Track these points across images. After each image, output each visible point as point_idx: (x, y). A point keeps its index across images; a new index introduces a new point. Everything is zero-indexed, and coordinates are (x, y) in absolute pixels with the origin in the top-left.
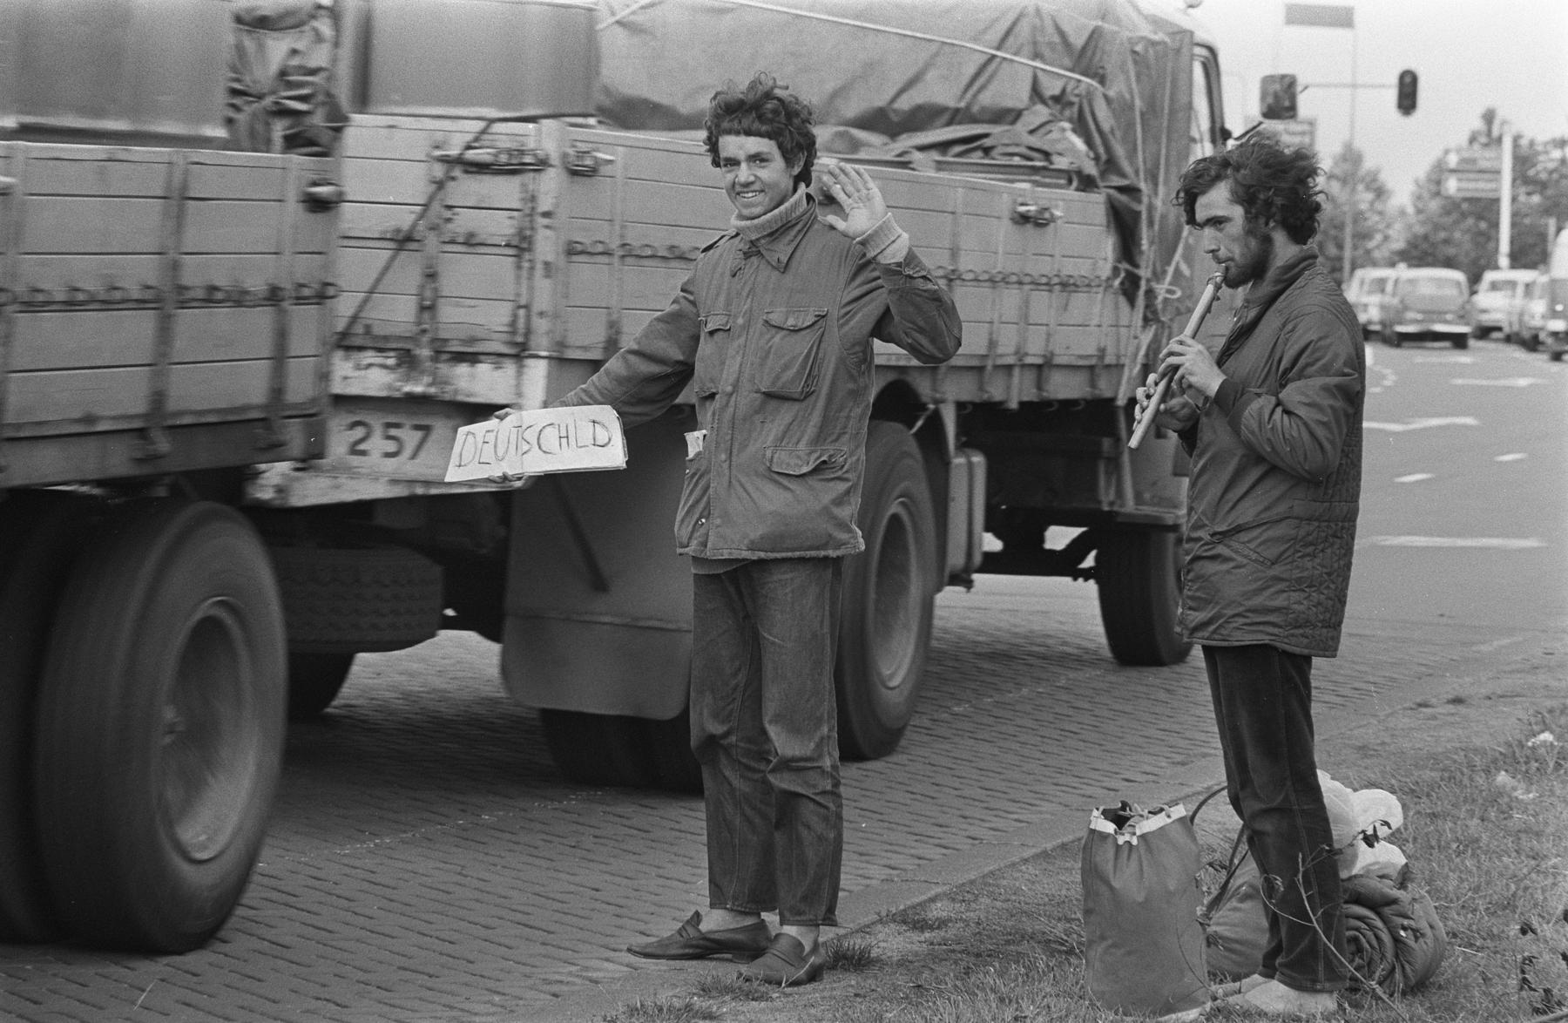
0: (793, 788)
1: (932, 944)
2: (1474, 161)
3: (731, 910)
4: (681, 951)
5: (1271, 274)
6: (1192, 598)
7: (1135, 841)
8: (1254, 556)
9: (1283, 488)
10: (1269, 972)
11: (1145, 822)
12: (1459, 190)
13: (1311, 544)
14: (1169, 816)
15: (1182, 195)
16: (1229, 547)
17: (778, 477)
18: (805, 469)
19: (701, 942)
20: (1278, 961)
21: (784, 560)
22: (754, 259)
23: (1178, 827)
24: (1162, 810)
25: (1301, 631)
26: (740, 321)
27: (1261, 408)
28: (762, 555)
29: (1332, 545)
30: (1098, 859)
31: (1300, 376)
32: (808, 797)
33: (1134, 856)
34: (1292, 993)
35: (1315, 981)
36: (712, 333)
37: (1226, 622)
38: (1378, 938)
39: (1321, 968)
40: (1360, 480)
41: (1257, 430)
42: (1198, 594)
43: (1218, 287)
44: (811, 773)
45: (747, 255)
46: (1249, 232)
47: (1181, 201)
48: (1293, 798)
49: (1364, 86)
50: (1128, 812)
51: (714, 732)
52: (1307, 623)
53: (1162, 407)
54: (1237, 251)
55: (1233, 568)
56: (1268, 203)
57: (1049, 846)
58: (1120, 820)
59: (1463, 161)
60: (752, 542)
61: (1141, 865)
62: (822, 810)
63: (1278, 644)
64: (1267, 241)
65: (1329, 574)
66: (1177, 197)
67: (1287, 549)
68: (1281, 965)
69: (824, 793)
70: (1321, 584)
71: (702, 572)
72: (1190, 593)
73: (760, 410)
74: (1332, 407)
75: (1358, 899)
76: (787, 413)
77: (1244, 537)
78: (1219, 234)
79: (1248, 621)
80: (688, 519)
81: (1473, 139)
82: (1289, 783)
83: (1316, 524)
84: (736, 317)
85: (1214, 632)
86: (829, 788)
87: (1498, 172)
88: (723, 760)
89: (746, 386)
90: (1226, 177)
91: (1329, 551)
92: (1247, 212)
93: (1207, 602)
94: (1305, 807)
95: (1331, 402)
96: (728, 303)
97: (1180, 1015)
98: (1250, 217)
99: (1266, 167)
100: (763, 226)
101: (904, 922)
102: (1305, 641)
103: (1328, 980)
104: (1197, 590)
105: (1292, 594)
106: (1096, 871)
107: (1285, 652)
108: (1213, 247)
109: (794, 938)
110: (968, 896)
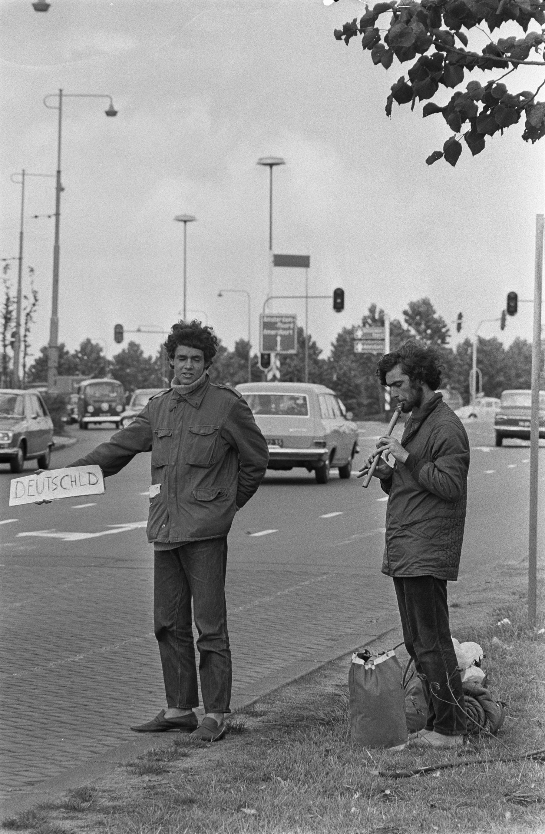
0: (209, 649)
1: (263, 722)
2: (371, 334)
3: (179, 708)
4: (155, 728)
5: (422, 406)
6: (393, 556)
7: (373, 668)
8: (423, 535)
9: (434, 502)
10: (430, 728)
11: (378, 659)
12: (363, 349)
13: (447, 529)
14: (388, 656)
15: (379, 372)
16: (410, 531)
17: (201, 504)
18: (212, 498)
19: (165, 724)
20: (434, 722)
21: (202, 541)
22: (183, 404)
23: (391, 661)
24: (384, 653)
25: (443, 569)
26: (177, 432)
27: (429, 469)
28: (197, 539)
29: (455, 529)
30: (357, 677)
31: (444, 454)
32: (216, 653)
33: (374, 675)
34: (443, 737)
35: (452, 731)
36: (161, 438)
37: (411, 566)
38: (477, 710)
39: (455, 725)
40: (466, 499)
41: (427, 479)
42: (395, 554)
43: (399, 413)
44: (217, 641)
45: (179, 401)
46: (412, 387)
47: (378, 374)
48: (440, 645)
49: (303, 297)
50: (368, 655)
51: (166, 625)
52: (446, 565)
53: (377, 467)
54: (407, 396)
55: (414, 541)
56: (420, 374)
57: (296, 677)
58: (366, 659)
59: (364, 334)
60: (192, 533)
61: (377, 678)
62: (223, 658)
63: (434, 575)
64: (420, 390)
65: (454, 542)
66: (377, 372)
67: (437, 532)
68: (436, 724)
69: (223, 650)
70: (451, 547)
71: (159, 550)
72: (391, 554)
73: (189, 473)
74: (459, 468)
75: (467, 693)
76: (202, 473)
77: (417, 526)
78: (398, 389)
79: (421, 565)
80: (155, 525)
81: (365, 323)
82: (438, 639)
83: (449, 519)
84: (174, 430)
85: (405, 570)
86: (225, 648)
87: (383, 340)
88: (169, 637)
89: (181, 462)
90: (399, 362)
91: (454, 532)
92: (410, 377)
93: (401, 557)
94: (446, 650)
95: (460, 466)
96: (169, 424)
97: (397, 747)
98: (412, 380)
99: (416, 356)
100: (192, 387)
101: (247, 713)
102: (445, 573)
103: (458, 730)
104: (395, 552)
105: (440, 552)
106: (356, 682)
107: (437, 579)
108: (396, 395)
109: (214, 720)
110: (270, 701)
